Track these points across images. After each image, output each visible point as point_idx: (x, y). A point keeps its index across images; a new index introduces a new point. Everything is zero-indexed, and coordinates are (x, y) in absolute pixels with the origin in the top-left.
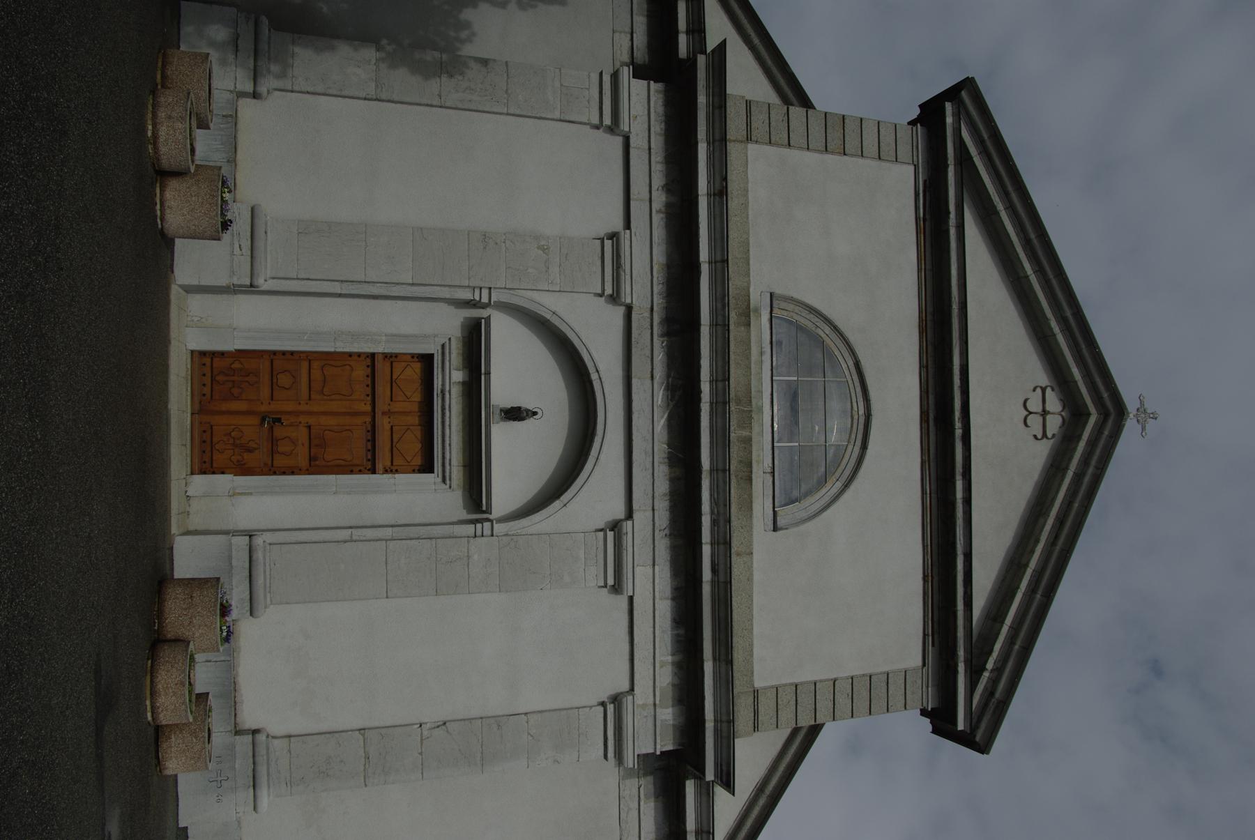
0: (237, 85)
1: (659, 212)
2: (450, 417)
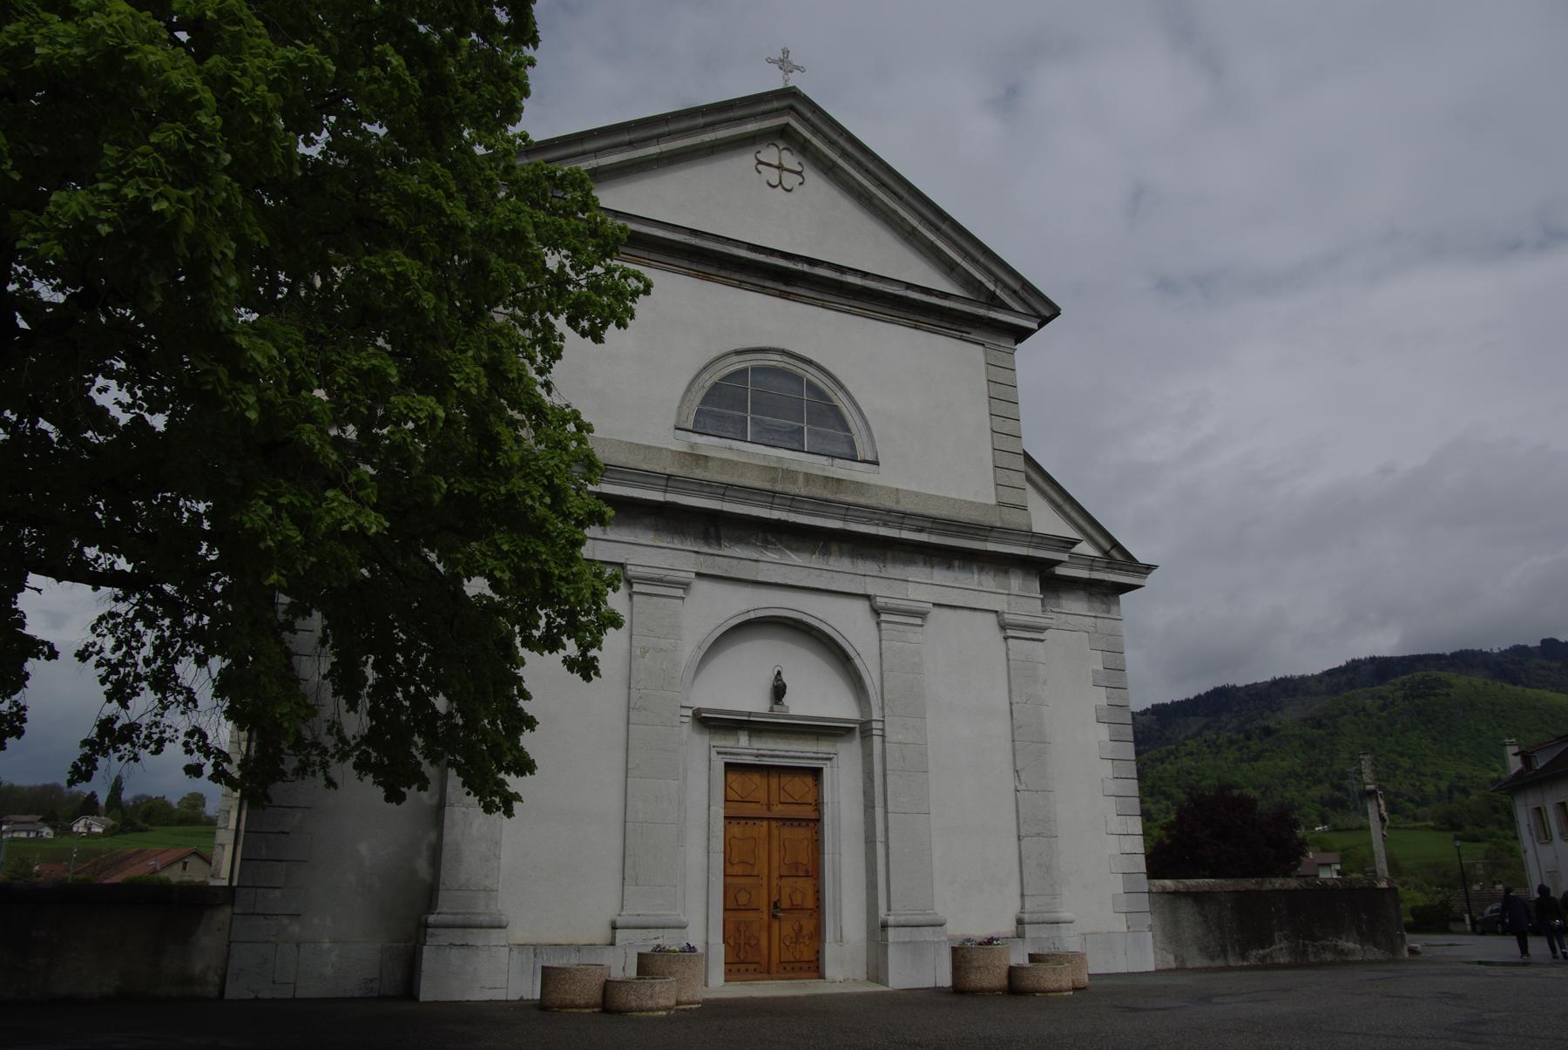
1: (605, 533)
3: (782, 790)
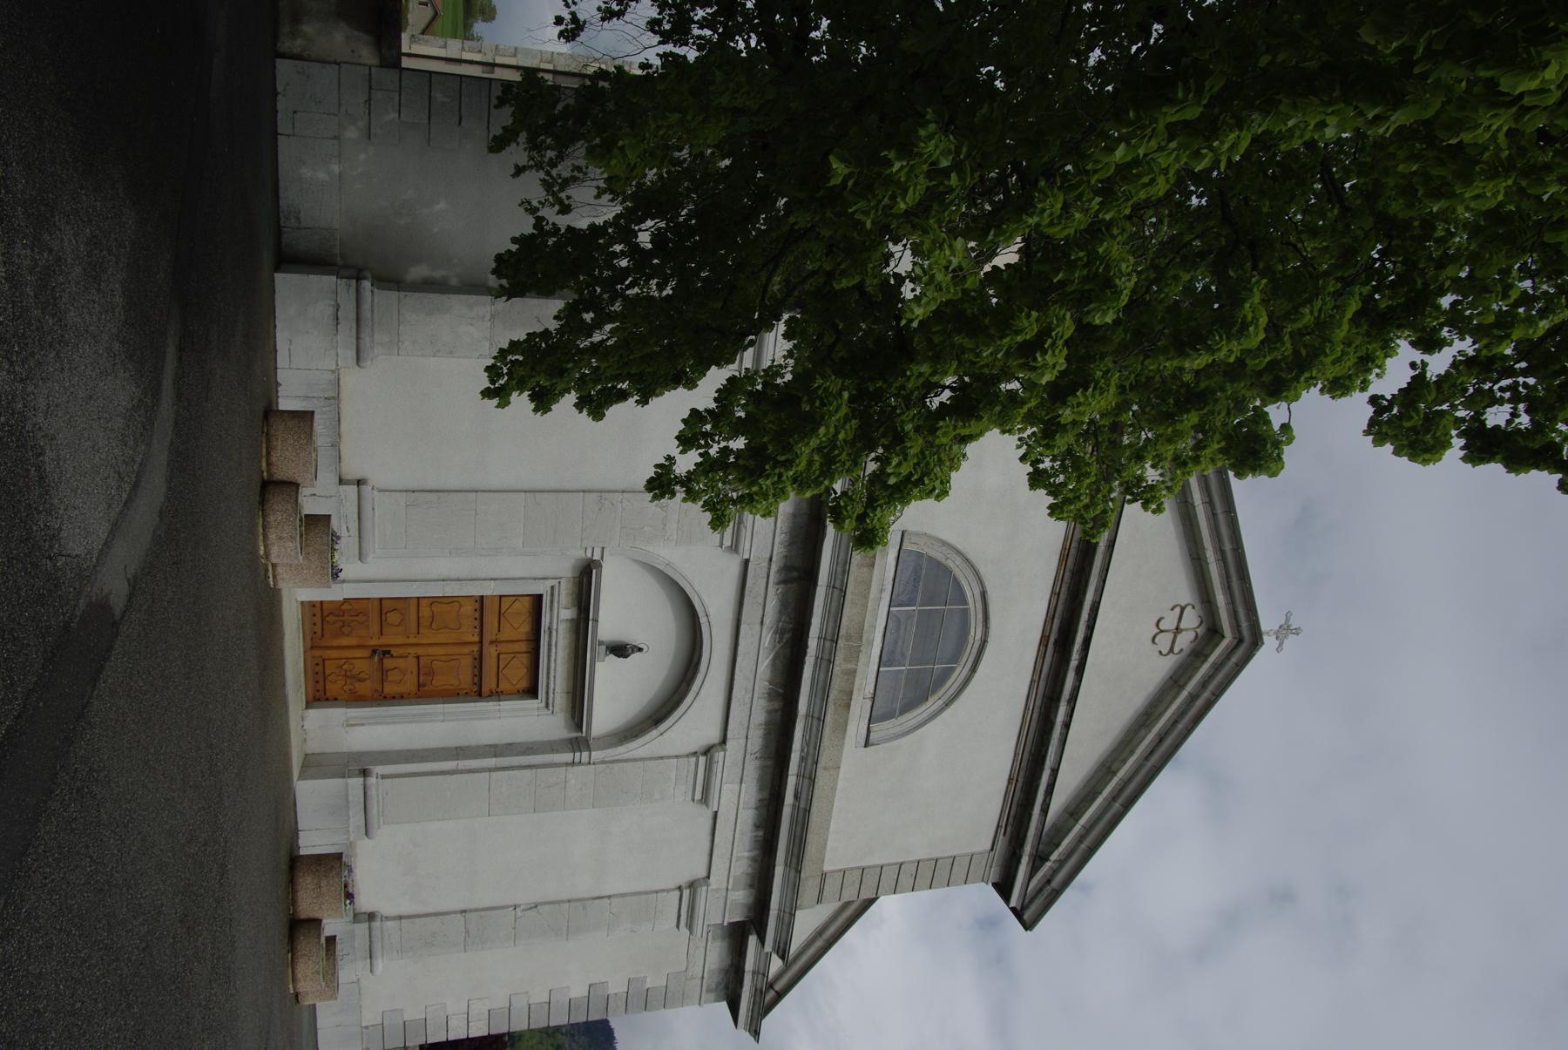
0: (339, 363)
2: (556, 653)
3: (513, 655)
